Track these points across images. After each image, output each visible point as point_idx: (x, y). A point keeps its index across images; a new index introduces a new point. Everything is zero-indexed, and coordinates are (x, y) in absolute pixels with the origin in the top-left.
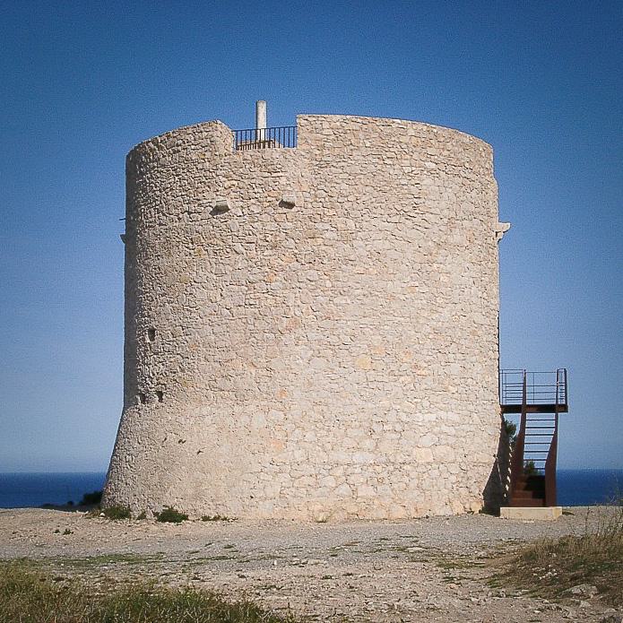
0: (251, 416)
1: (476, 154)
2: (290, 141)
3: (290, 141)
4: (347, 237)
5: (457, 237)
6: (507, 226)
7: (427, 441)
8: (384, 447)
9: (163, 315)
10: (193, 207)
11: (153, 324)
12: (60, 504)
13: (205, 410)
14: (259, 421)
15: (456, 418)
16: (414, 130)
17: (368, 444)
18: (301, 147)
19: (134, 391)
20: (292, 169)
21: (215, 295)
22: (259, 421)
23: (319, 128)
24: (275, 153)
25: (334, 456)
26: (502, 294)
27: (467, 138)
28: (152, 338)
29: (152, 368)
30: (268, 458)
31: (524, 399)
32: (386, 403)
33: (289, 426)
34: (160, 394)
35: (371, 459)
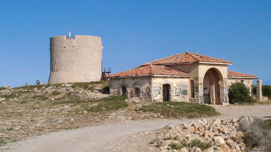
0: (69, 73)
1: (99, 39)
2: (74, 38)
3: (74, 38)
4: (81, 51)
5: (95, 50)
6: (103, 47)
7: (92, 76)
8: (86, 77)
9: (57, 60)
10: (61, 46)
11: (56, 62)
12: (182, 70)
13: (63, 73)
14: (70, 74)
15: (95, 73)
16: (90, 37)
17: (84, 77)
18: (75, 39)
19: (52, 69)
20: (74, 42)
21: (64, 58)
22: (70, 74)
23: (78, 37)
24: (72, 40)
25: (80, 78)
26: (102, 41)
27: (97, 37)
28: (55, 63)
29: (55, 67)
30: (72, 79)
31: (105, 71)
32: (86, 72)
33: (74, 75)
34: (57, 71)
35: (85, 79)
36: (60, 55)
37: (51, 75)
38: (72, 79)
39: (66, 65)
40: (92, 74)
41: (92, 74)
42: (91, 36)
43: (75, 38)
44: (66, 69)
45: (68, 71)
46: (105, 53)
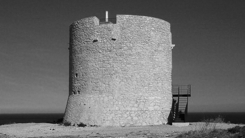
0: (104, 98)
1: (166, 26)
4: (130, 49)
5: (160, 48)
6: (174, 45)
9: (79, 69)
10: (88, 40)
11: (77, 72)
13: (91, 96)
14: (106, 99)
15: (160, 98)
16: (148, 19)
17: (136, 105)
18: (118, 24)
19: (72, 91)
20: (115, 29)
22: (106, 99)
24: (111, 25)
25: (127, 109)
28: (77, 76)
29: (77, 85)
30: (108, 109)
32: (141, 94)
34: (79, 92)
36: (86, 59)
37: (69, 108)
38: (108, 109)
39: (97, 79)
40: (154, 98)
41: (154, 98)
42: (151, 18)
43: (118, 20)
44: (98, 89)
45: (101, 92)
46: (180, 55)
